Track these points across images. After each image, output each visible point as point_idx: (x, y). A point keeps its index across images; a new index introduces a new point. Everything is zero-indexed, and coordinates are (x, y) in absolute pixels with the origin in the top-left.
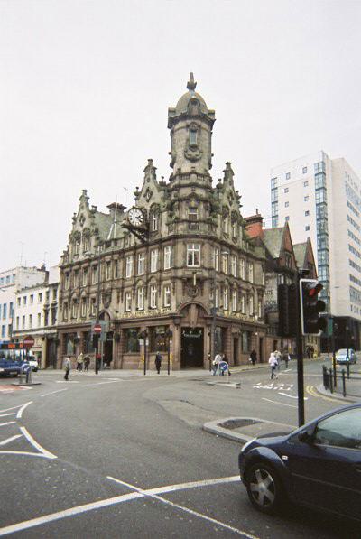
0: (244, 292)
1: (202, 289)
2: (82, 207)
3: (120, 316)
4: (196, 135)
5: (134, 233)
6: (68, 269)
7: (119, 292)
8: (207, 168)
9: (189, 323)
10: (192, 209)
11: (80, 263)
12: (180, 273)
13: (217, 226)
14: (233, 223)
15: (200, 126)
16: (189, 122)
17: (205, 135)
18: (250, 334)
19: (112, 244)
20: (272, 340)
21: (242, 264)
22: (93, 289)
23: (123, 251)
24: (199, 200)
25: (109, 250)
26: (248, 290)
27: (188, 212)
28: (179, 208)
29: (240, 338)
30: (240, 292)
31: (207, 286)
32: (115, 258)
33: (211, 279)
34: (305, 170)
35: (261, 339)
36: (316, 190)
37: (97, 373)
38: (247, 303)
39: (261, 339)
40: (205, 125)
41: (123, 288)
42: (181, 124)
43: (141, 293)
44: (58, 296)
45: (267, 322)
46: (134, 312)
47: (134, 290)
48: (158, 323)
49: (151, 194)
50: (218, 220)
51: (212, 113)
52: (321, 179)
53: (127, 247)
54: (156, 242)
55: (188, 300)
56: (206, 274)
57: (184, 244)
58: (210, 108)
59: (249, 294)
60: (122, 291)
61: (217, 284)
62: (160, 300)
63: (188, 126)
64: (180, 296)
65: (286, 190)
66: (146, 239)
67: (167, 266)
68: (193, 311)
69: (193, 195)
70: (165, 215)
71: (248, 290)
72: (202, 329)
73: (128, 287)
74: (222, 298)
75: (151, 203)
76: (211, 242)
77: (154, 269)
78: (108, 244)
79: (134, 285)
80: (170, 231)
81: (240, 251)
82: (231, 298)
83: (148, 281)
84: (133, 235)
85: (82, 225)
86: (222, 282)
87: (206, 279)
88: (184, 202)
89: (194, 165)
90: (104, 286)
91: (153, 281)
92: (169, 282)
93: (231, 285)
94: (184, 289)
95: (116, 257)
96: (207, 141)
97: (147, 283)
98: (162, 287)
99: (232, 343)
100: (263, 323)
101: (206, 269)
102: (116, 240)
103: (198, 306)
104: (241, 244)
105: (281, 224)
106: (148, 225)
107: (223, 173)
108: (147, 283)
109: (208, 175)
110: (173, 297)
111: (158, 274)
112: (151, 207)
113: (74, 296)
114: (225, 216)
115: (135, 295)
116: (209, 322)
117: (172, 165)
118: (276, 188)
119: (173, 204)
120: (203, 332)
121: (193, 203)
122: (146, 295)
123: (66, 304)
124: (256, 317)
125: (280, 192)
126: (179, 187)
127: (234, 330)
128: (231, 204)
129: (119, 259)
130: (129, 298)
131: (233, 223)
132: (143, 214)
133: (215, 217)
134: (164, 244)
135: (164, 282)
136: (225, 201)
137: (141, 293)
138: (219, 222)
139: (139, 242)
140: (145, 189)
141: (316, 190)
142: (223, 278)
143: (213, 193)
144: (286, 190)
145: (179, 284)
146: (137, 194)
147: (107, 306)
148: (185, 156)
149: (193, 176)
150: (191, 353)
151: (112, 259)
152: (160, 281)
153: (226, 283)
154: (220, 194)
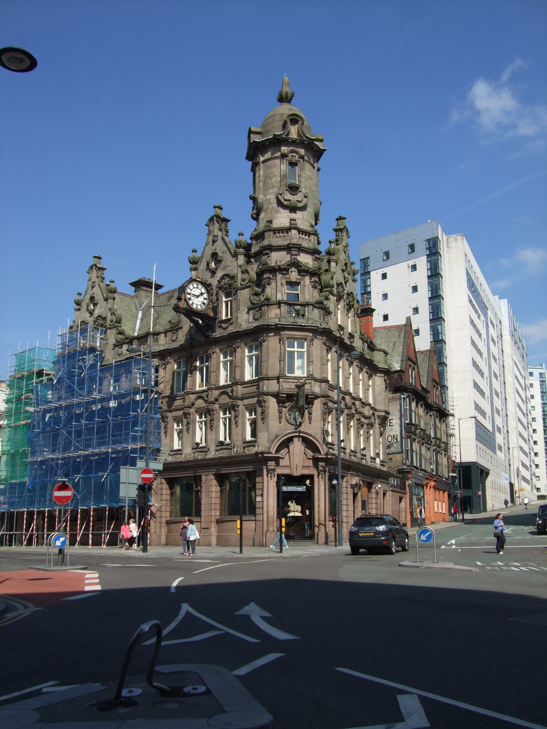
10: (292, 284)
14: (348, 310)
24: (303, 271)
27: (286, 290)
37: (145, 550)
50: (331, 303)
68: (297, 446)
69: (296, 264)
72: (311, 477)
75: (219, 274)
89: (293, 216)
101: (316, 380)
103: (309, 443)
106: (216, 310)
109: (316, 234)
120: (312, 482)
121: (294, 275)
131: (348, 310)
133: (327, 299)
136: (339, 277)
140: (88, 297)
146: (194, 262)
149: (294, 232)
150: (393, 543)
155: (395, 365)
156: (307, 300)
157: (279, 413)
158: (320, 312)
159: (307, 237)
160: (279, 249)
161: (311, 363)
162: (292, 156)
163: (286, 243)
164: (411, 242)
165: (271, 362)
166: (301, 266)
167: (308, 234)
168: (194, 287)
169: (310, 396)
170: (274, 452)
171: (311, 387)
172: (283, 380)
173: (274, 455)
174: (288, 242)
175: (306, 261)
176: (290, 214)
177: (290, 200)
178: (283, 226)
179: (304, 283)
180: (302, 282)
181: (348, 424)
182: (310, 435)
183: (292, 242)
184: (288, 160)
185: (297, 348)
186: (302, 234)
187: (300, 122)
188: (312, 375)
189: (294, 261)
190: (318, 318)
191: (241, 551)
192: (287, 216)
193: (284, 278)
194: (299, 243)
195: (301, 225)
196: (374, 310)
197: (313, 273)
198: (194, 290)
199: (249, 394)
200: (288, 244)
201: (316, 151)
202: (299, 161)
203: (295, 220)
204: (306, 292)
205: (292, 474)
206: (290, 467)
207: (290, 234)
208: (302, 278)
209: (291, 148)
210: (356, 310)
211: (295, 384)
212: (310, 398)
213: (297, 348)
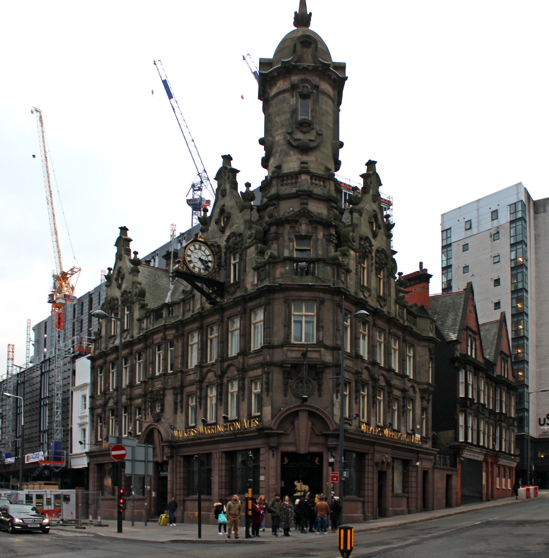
0: (397, 393)
1: (320, 386)
2: (119, 257)
3: (179, 434)
4: (310, 102)
5: (200, 290)
6: (100, 361)
7: (175, 395)
8: (332, 166)
9: (295, 444)
10: (300, 238)
11: (116, 349)
12: (278, 356)
13: (348, 271)
15: (317, 87)
16: (295, 78)
17: (326, 104)
18: (406, 464)
19: (165, 313)
20: (445, 473)
21: (395, 345)
22: (138, 391)
23: (182, 324)
25: (161, 323)
26: (404, 391)
28: (277, 238)
29: (390, 472)
30: (390, 393)
31: (329, 378)
32: (170, 337)
33: (337, 366)
34: (495, 214)
35: (425, 473)
36: (512, 245)
38: (403, 412)
39: (425, 473)
40: (325, 86)
41: (182, 387)
42: (282, 85)
43: (213, 393)
44: (88, 406)
45: (434, 445)
46: (201, 428)
47: (201, 389)
48: (240, 446)
49: (229, 218)
51: (342, 67)
52: (519, 228)
53: (188, 315)
54: (236, 303)
55: (294, 402)
56: (328, 358)
57: (287, 303)
58: (336, 58)
59: (406, 398)
60: (182, 393)
61: (347, 375)
62: (244, 406)
63: (294, 87)
64: (278, 396)
65: (465, 247)
66: (218, 300)
67: (257, 342)
68: (303, 422)
69: (305, 214)
70: (252, 252)
71: (404, 391)
73: (191, 384)
74: (357, 402)
76: (337, 299)
77: (234, 349)
78: (157, 313)
79: (201, 381)
80: (260, 280)
81: (390, 320)
82: (374, 403)
83: (224, 373)
84: (198, 294)
85: (119, 287)
86: (358, 373)
87: (326, 366)
88: (288, 227)
89: (305, 158)
90: (153, 386)
91: (233, 372)
92: (259, 372)
93: (375, 380)
94: (286, 384)
95: (171, 334)
96: (331, 118)
97: (221, 377)
98: (246, 382)
99: (376, 480)
100: (428, 445)
101: (326, 347)
102: (169, 306)
103: (312, 415)
104: (393, 309)
105: (458, 287)
107: (361, 180)
108: (221, 377)
110: (266, 399)
111: (240, 359)
112: (227, 241)
113: (111, 403)
114: (363, 255)
115: (202, 399)
116: (332, 442)
117: (265, 163)
118: (450, 245)
119: (266, 232)
121: (304, 229)
122: (222, 398)
123: (99, 416)
124: (418, 436)
125: (456, 249)
126: (278, 198)
127: (378, 457)
128: (375, 236)
129: (176, 337)
130: (192, 403)
132: (213, 253)
134: (250, 304)
135: (251, 374)
136: (365, 230)
137: (213, 393)
138: (352, 265)
139: (208, 306)
140: (218, 210)
141: (512, 245)
142: (360, 367)
143: (342, 213)
144: (465, 247)
145: (277, 377)
147: (158, 419)
148: (289, 143)
151: (164, 339)
152: (243, 370)
153: (365, 376)
154: (356, 215)
155: (451, 336)
156: (320, 257)
157: (285, 385)
158: (333, 270)
159: (322, 183)
160: (290, 197)
161: (321, 329)
162: (304, 87)
163: (294, 190)
164: (493, 209)
165: (275, 328)
166: (312, 217)
167: (314, 178)
168: (195, 248)
169: (318, 366)
170: (275, 428)
171: (321, 355)
172: (288, 348)
173: (275, 431)
174: (298, 189)
175: (319, 211)
176: (300, 157)
177: (299, 140)
178: (292, 170)
179: (317, 236)
180: (314, 235)
181: (374, 397)
182: (318, 409)
183: (302, 188)
184: (299, 92)
185: (306, 312)
186: (316, 180)
187: (313, 46)
188: (322, 342)
189: (304, 211)
190: (331, 276)
191: (120, 530)
192: (297, 159)
193: (292, 232)
194: (311, 189)
195: (314, 168)
196: (431, 276)
197: (326, 225)
198: (196, 251)
199: (254, 366)
200: (298, 191)
201: (335, 81)
202: (312, 93)
203: (307, 163)
204: (320, 248)
205: (298, 452)
206: (295, 444)
207: (299, 180)
208: (314, 231)
209: (303, 77)
210: (390, 270)
211: (301, 352)
212: (320, 368)
213: (306, 312)
